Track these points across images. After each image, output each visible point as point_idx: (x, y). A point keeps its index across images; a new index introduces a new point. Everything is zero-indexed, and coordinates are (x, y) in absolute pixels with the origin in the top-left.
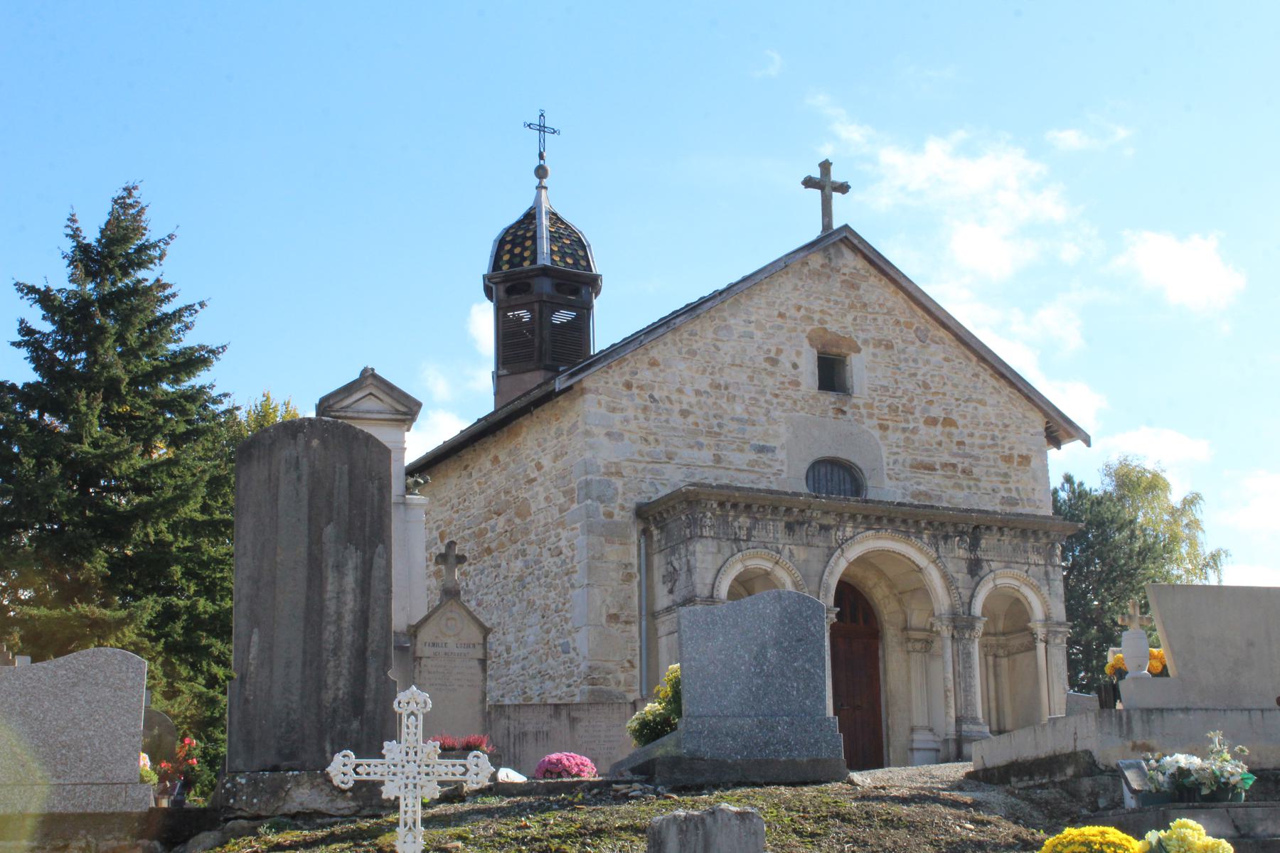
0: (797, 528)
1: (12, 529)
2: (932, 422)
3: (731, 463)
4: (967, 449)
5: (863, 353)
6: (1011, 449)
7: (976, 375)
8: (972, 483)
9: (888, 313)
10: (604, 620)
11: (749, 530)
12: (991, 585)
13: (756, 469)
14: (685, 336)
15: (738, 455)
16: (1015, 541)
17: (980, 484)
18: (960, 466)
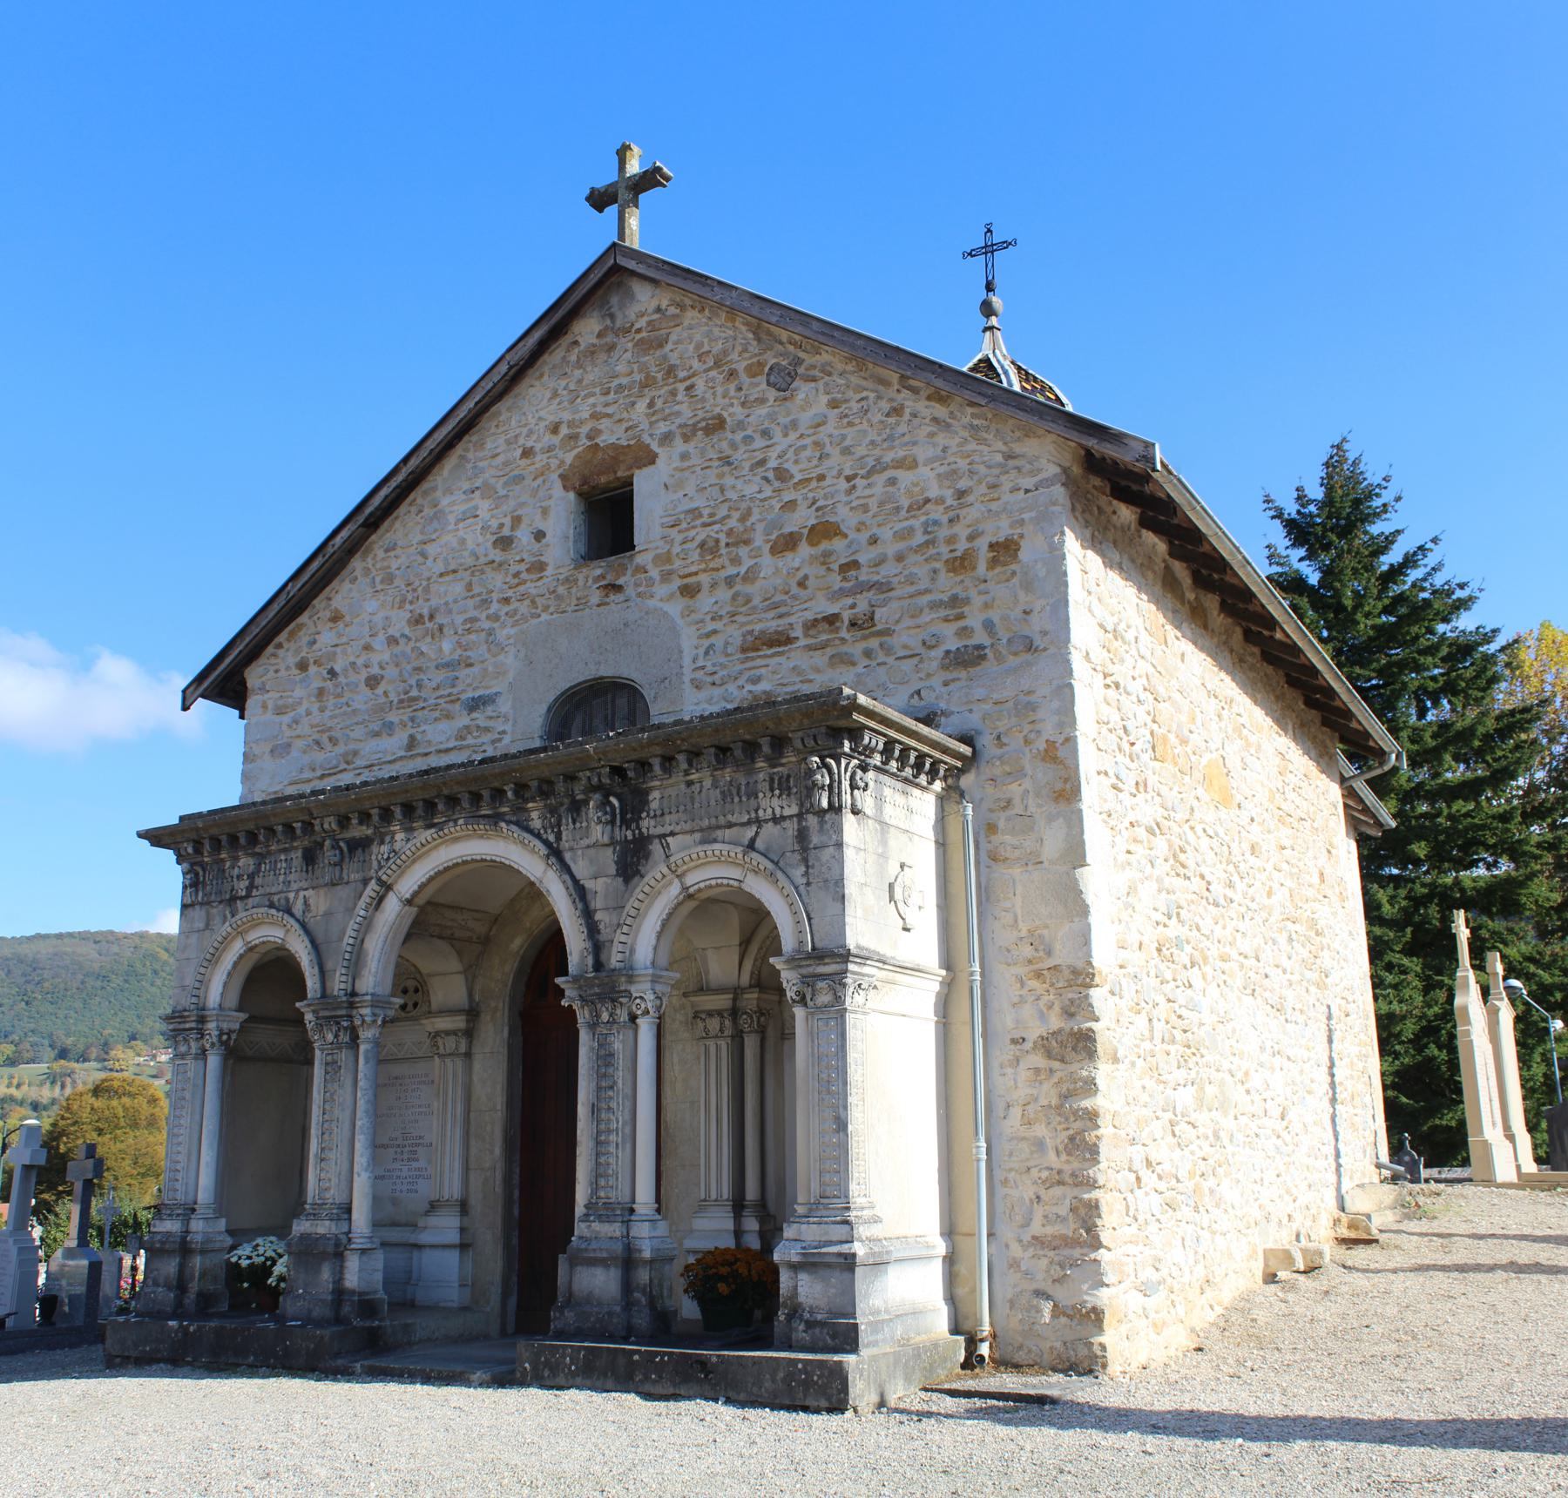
1: (1560, 801)
2: (787, 543)
3: (429, 742)
4: (864, 575)
5: (661, 462)
6: (971, 538)
7: (897, 411)
8: (874, 643)
9: (717, 364)
12: (675, 889)
13: (470, 741)
14: (381, 554)
15: (443, 725)
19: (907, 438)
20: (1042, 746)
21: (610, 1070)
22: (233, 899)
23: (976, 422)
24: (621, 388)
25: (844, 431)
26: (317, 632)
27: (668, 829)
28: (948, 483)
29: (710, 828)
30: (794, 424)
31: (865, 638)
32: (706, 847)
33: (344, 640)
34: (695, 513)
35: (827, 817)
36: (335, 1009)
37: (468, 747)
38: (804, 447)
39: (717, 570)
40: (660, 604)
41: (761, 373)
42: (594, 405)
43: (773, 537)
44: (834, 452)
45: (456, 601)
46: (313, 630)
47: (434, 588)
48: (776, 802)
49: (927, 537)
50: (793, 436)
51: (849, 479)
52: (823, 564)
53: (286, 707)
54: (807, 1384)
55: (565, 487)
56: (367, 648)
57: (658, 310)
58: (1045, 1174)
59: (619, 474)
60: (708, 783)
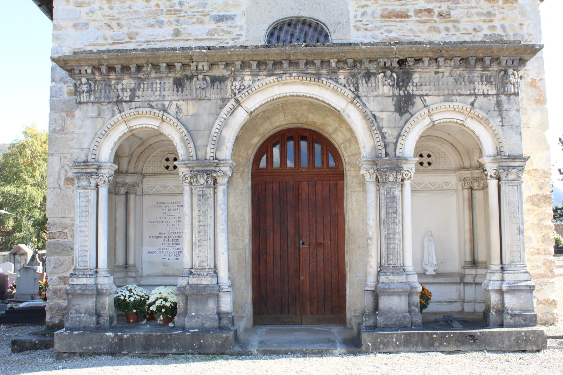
0: (187, 83)
3: (189, 34)
8: (450, 25)
10: (62, 183)
11: (133, 90)
12: (427, 121)
13: (216, 36)
15: (198, 26)
16: (458, 72)
17: (459, 26)
18: (436, 11)
20: (530, 80)
22: (119, 102)
27: (424, 93)
29: (448, 95)
31: (446, 22)
32: (446, 104)
35: (512, 97)
36: (206, 166)
37: (216, 39)
48: (484, 87)
54: (526, 341)
58: (532, 250)
60: (447, 74)
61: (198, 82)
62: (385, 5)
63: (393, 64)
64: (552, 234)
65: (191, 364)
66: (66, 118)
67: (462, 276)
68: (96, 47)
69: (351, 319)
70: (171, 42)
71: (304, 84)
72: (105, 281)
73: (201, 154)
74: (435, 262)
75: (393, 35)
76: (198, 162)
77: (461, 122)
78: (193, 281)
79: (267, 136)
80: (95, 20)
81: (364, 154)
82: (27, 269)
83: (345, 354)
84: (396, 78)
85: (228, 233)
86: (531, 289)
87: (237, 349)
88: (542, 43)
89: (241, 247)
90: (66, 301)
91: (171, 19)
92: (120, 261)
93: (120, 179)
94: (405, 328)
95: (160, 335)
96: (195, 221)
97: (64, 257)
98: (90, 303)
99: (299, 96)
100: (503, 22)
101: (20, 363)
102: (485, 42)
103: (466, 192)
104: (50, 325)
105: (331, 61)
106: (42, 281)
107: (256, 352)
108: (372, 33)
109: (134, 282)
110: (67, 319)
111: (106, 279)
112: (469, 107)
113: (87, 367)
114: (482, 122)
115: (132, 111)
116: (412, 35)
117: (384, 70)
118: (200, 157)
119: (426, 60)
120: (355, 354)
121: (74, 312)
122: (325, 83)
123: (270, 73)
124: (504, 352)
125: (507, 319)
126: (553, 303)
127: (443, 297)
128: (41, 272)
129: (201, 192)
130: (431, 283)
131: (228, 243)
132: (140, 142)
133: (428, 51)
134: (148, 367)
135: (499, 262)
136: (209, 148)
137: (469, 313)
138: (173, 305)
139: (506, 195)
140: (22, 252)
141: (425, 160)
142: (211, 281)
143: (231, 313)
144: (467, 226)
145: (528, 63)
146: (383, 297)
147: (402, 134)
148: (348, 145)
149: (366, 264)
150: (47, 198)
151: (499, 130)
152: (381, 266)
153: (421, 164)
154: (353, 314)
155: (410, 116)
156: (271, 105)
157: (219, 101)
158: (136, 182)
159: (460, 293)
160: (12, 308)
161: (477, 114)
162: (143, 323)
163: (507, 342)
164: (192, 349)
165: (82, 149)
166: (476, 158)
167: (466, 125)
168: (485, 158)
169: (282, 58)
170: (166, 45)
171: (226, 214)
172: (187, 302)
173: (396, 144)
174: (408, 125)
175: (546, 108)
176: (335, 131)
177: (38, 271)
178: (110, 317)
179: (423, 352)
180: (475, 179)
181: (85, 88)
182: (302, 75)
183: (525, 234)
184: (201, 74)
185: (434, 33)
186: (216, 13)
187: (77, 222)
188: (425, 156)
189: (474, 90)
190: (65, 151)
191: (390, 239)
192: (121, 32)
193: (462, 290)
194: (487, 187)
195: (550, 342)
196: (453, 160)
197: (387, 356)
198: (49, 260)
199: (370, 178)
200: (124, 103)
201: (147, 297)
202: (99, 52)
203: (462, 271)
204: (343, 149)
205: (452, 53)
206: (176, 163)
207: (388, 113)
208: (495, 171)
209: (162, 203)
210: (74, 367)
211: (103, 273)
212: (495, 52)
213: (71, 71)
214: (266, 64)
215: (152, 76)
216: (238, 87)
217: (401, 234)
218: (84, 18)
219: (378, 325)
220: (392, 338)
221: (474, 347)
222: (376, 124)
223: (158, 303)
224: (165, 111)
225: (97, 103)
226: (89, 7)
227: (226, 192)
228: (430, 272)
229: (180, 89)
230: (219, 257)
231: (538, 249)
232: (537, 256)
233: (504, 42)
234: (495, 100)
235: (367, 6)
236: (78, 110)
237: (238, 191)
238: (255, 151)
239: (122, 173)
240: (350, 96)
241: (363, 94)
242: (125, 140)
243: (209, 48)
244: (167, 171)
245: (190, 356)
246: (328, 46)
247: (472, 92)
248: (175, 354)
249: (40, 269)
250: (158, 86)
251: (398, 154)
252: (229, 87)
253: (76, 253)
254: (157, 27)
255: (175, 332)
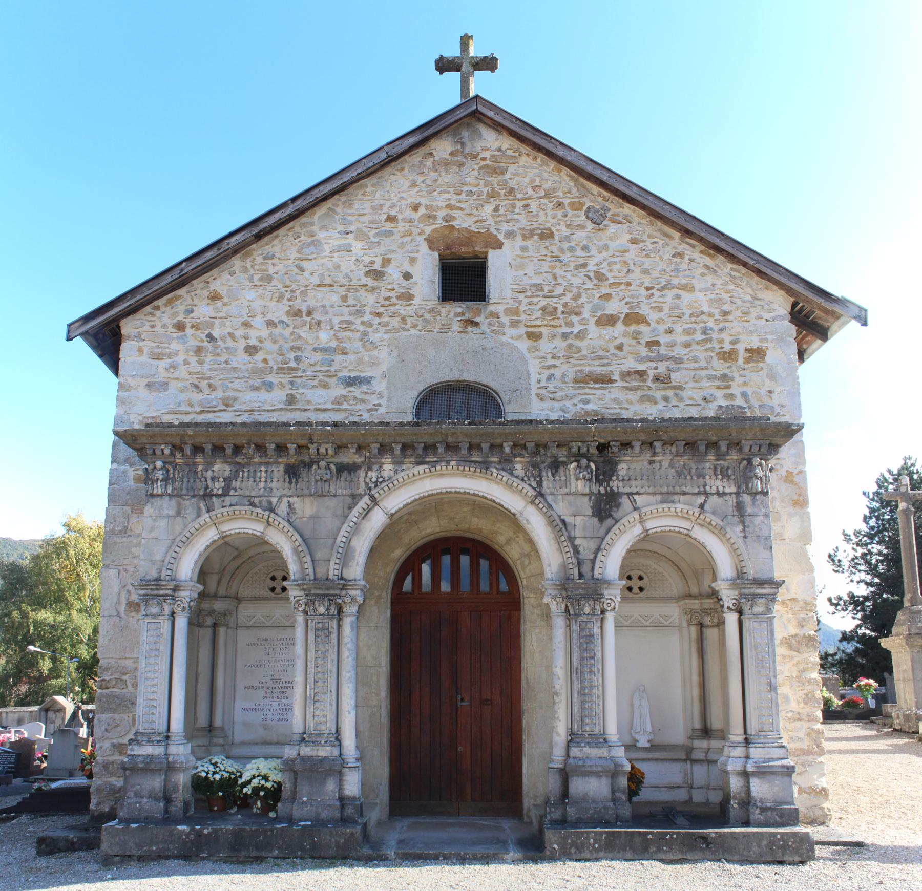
2: (611, 320)
3: (308, 402)
4: (663, 351)
6: (734, 342)
7: (680, 255)
8: (670, 393)
9: (547, 195)
10: (122, 608)
11: (228, 480)
12: (637, 530)
13: (345, 406)
15: (320, 391)
17: (684, 394)
18: (651, 373)
19: (687, 273)
20: (784, 473)
21: (592, 646)
23: (733, 273)
24: (470, 193)
25: (643, 259)
26: (195, 303)
27: (634, 490)
28: (717, 305)
29: (668, 493)
30: (606, 247)
31: (664, 389)
32: (665, 506)
33: (222, 315)
34: (539, 287)
35: (758, 497)
36: (328, 589)
37: (345, 410)
38: (615, 263)
39: (555, 327)
40: (511, 341)
41: (581, 210)
42: (449, 199)
43: (598, 314)
44: (637, 271)
45: (332, 306)
46: (189, 301)
47: (311, 294)
48: (718, 483)
49: (704, 337)
50: (605, 254)
51: (648, 289)
52: (635, 338)
53: (164, 355)
54: (784, 848)
55: (430, 248)
56: (246, 324)
57: (499, 150)
58: (789, 715)
59: (477, 249)
60: (666, 464)
61: (319, 471)
62: (580, 365)
63: (591, 450)
64: (819, 692)
65: (300, 872)
66: (131, 515)
67: (689, 750)
68: (177, 416)
69: (529, 810)
70: (283, 413)
71: (466, 476)
72: (180, 751)
73: (321, 572)
74: (649, 729)
75: (590, 407)
76: (316, 582)
77: (685, 532)
78: (306, 751)
79: (414, 548)
80: (177, 379)
81: (548, 575)
82: (65, 732)
83: (521, 861)
84: (594, 468)
85: (357, 683)
86: (789, 771)
87: (366, 851)
88: (802, 421)
89: (374, 704)
90: (122, 779)
91: (283, 381)
92: (203, 721)
93: (205, 605)
94: (608, 824)
95: (256, 830)
96: (311, 665)
97: (122, 715)
98: (156, 783)
99: (459, 493)
100: (745, 389)
101: (49, 871)
102: (719, 418)
103: (694, 630)
104: (96, 814)
105: (505, 444)
106: (86, 749)
107: (394, 857)
108: (561, 404)
109: (222, 753)
110: (122, 805)
111: (181, 747)
112: (697, 510)
113: (149, 876)
114: (716, 531)
115: (225, 509)
116: (617, 406)
117: (578, 458)
118: (319, 575)
119: (637, 445)
120: (535, 861)
121: (132, 795)
122: (495, 475)
123: (420, 460)
124: (752, 863)
125: (756, 814)
126: (823, 793)
127: (662, 779)
128: (85, 736)
129: (320, 625)
130: (643, 760)
131: (357, 697)
132: (236, 553)
133: (639, 431)
134: (237, 877)
135: (741, 731)
136: (332, 563)
137: (699, 804)
138: (275, 786)
139: (750, 635)
140: (58, 707)
141: (635, 583)
142: (332, 752)
143: (359, 798)
144: (695, 678)
145: (780, 449)
146: (575, 778)
147: (602, 547)
148: (527, 562)
149: (551, 730)
150: (101, 630)
151: (740, 542)
152: (572, 734)
153: (630, 589)
154: (532, 802)
155: (613, 522)
156: (419, 504)
157: (347, 498)
158: (228, 610)
159: (686, 774)
160: (40, 789)
161: (708, 520)
162: (232, 811)
163: (755, 848)
164: (301, 851)
165: (153, 562)
166: (707, 582)
167: (693, 536)
168: (719, 582)
169: (437, 440)
170: (275, 417)
171: (354, 656)
172: (296, 782)
173: (593, 561)
174: (610, 535)
175: (808, 513)
176: (508, 542)
177: (81, 735)
178: (185, 803)
179: (633, 860)
180: (706, 612)
181: (160, 475)
182: (463, 463)
183: (779, 691)
184: (323, 459)
185: (648, 405)
186: (345, 373)
187: (142, 665)
188: (635, 578)
189: (705, 486)
190: (126, 562)
191: (585, 695)
192: (212, 397)
193: (689, 771)
194: (724, 623)
195: (819, 851)
196: (675, 585)
197: (582, 864)
198: (99, 720)
199: (557, 608)
200: (214, 498)
201: (239, 774)
202: (183, 425)
203: (688, 743)
204: (519, 567)
205: (672, 435)
206: (285, 583)
207: (582, 517)
208: (734, 601)
209: (265, 640)
210: (129, 877)
211: (177, 738)
212: (734, 433)
213: (141, 451)
214: (413, 447)
215: (256, 460)
216: (374, 480)
217: (601, 688)
218: (162, 375)
219: (569, 819)
220: (588, 838)
221: (708, 853)
222: (566, 534)
223: (255, 782)
224: (272, 510)
225: (176, 496)
226: (169, 361)
227: (355, 625)
228: (643, 742)
229: (294, 480)
230: (343, 718)
231: (799, 714)
232: (798, 724)
233: (746, 419)
234: (735, 501)
235: (555, 366)
236: (149, 505)
237: (371, 624)
238: (397, 568)
239: (208, 596)
240: (529, 494)
241: (548, 491)
242: (215, 549)
243: (335, 425)
244: (273, 595)
245: (298, 861)
246: (500, 424)
247: (702, 489)
248: (277, 858)
249: (83, 732)
250: (263, 474)
251: (596, 575)
252: (361, 479)
253: (140, 710)
254: (263, 390)
255: (278, 826)
